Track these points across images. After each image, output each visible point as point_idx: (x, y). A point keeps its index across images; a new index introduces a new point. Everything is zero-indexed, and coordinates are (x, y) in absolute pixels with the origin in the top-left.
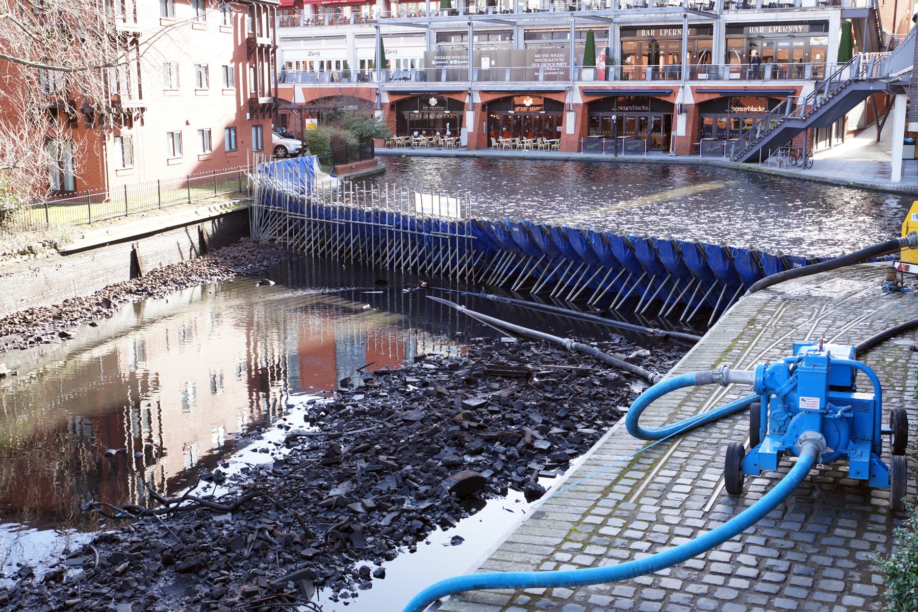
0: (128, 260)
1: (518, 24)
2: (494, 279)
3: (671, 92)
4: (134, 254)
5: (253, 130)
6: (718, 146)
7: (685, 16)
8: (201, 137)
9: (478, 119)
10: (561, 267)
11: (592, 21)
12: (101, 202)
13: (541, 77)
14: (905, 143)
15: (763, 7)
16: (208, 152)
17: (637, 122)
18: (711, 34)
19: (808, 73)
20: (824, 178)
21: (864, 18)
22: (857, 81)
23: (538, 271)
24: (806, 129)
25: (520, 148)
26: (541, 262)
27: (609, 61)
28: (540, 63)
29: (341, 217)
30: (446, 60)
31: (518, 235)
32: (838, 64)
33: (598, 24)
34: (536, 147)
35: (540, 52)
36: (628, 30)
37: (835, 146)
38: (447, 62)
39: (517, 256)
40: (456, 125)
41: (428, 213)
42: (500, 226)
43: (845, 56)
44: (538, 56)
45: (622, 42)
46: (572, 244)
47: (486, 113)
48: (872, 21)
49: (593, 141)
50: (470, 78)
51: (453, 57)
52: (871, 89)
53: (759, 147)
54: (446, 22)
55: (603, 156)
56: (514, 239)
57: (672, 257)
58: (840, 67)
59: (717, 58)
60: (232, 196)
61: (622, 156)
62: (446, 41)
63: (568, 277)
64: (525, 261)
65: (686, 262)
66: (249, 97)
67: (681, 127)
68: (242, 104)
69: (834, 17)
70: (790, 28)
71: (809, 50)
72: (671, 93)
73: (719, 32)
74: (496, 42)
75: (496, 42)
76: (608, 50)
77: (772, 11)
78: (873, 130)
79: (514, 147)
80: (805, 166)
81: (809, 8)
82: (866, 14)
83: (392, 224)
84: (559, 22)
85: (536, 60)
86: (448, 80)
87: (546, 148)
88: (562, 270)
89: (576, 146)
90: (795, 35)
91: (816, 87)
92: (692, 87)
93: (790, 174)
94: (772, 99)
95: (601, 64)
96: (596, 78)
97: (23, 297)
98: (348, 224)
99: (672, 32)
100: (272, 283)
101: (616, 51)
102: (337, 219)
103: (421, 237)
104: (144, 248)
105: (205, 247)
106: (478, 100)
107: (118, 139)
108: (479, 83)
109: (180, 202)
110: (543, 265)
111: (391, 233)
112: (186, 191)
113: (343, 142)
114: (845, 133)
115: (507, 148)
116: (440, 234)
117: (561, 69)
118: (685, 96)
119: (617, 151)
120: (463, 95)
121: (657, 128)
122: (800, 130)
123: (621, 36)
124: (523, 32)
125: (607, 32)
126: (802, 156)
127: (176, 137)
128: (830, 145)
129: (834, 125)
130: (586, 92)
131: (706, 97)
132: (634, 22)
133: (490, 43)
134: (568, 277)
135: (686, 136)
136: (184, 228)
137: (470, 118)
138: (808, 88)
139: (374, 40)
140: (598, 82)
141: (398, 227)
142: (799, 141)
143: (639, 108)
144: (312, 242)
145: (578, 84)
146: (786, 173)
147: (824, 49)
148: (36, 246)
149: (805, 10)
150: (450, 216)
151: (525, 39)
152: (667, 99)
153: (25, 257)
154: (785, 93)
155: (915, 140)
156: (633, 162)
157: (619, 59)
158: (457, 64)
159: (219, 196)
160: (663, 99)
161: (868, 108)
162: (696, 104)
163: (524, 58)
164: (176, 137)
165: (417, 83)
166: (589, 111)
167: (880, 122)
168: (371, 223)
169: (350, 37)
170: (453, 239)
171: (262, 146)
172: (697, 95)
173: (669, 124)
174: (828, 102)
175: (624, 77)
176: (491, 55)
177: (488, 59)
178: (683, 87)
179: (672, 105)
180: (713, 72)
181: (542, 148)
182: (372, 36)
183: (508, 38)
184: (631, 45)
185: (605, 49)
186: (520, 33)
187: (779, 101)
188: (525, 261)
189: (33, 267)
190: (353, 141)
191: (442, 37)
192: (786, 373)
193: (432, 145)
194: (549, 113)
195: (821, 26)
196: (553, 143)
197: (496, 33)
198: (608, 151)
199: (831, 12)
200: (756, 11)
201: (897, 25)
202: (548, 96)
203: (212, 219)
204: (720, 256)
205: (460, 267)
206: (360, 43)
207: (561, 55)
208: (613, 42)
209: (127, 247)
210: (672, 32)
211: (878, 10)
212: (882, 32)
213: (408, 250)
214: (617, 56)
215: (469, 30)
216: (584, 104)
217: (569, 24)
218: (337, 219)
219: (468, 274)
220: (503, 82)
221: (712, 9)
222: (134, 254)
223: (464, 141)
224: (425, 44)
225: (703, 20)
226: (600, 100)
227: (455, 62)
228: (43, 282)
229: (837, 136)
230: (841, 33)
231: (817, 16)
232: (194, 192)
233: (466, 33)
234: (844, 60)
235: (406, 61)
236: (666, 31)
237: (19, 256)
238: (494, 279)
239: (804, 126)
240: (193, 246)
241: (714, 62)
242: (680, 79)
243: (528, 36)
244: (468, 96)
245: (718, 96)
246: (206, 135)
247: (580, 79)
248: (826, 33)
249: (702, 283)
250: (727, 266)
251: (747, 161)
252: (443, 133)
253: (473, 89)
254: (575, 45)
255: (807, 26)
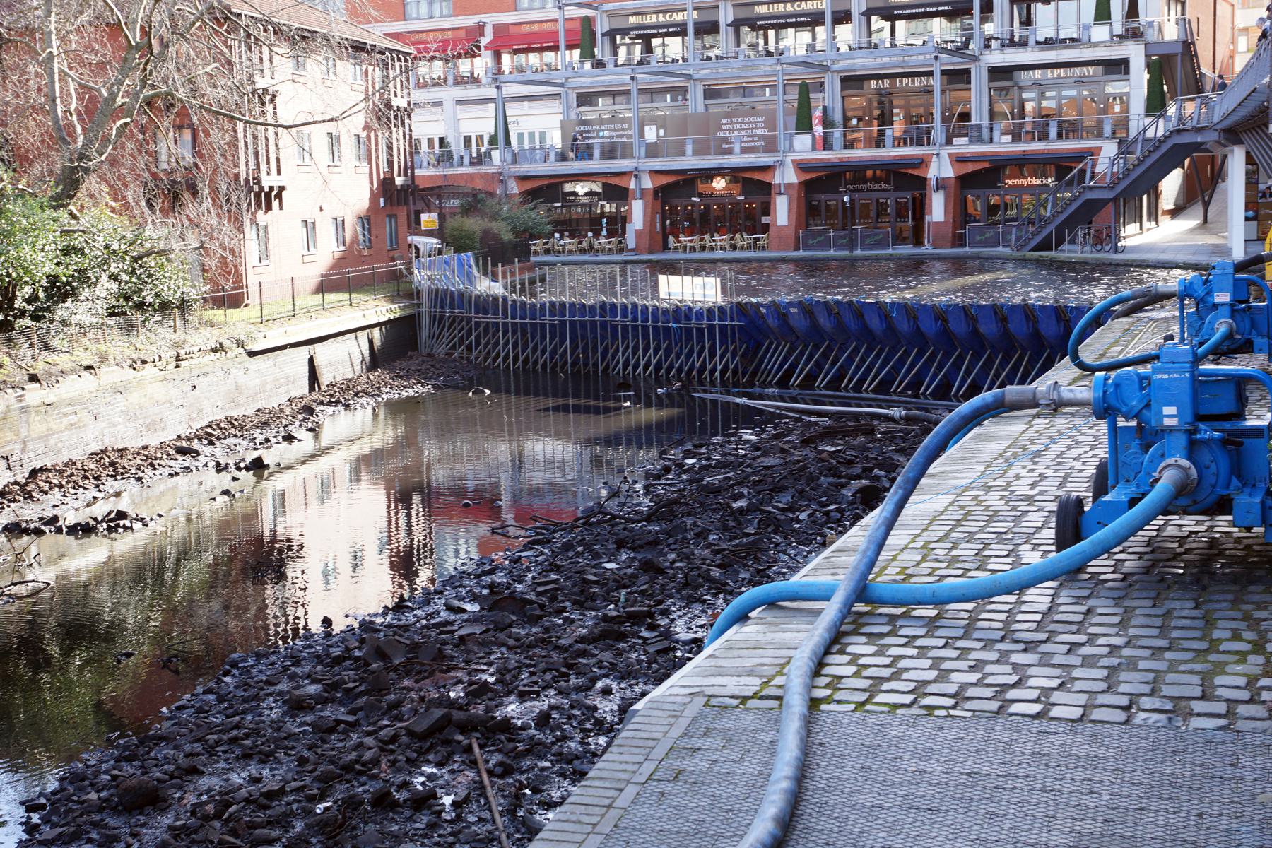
0: (306, 369)
1: (696, 77)
2: (764, 376)
3: (922, 163)
4: (311, 361)
5: (387, 220)
6: (990, 234)
7: (936, 58)
8: (334, 228)
9: (649, 210)
10: (849, 356)
11: (801, 69)
12: (239, 307)
13: (737, 148)
14: (1247, 219)
15: (1038, 43)
16: (342, 248)
17: (873, 208)
18: (969, 82)
19: (1107, 130)
20: (1144, 261)
21: (1177, 54)
22: (1178, 132)
23: (819, 366)
24: (1115, 199)
25: (712, 249)
26: (823, 353)
27: (827, 123)
28: (729, 130)
29: (552, 314)
30: (594, 131)
31: (796, 317)
32: (1147, 116)
33: (810, 73)
34: (734, 247)
35: (728, 115)
36: (852, 82)
37: (1148, 230)
38: (594, 135)
39: (792, 343)
40: (618, 224)
41: (676, 297)
42: (772, 308)
43: (1156, 105)
44: (725, 121)
45: (843, 98)
46: (868, 322)
47: (659, 203)
48: (1187, 58)
49: (814, 235)
50: (636, 154)
51: (603, 127)
52: (1199, 140)
53: (1051, 228)
54: (589, 78)
55: (832, 252)
56: (791, 322)
57: (994, 325)
58: (1148, 120)
59: (979, 117)
60: (392, 299)
61: (858, 252)
62: (591, 105)
63: (858, 368)
64: (802, 354)
65: (1011, 330)
66: (382, 177)
67: (937, 209)
68: (375, 185)
69: (1135, 54)
70: (1077, 71)
71: (1107, 101)
72: (921, 163)
73: (979, 80)
74: (663, 104)
75: (663, 104)
76: (825, 108)
77: (1051, 49)
78: (1198, 209)
79: (703, 248)
80: (1116, 251)
81: (1102, 42)
82: (1179, 49)
83: (627, 317)
84: (749, 73)
85: (724, 127)
86: (603, 157)
87: (749, 248)
88: (850, 360)
89: (792, 242)
90: (1084, 80)
91: (1119, 148)
92: (950, 155)
93: (1097, 259)
94: (1062, 166)
95: (818, 130)
96: (814, 148)
97: (218, 404)
98: (563, 323)
99: (913, 81)
100: (488, 392)
101: (836, 110)
102: (547, 317)
103: (667, 329)
104: (323, 353)
105: (376, 360)
106: (648, 184)
107: (254, 228)
108: (648, 160)
109: (335, 305)
110: (825, 356)
111: (625, 328)
112: (321, 295)
113: (496, 237)
114: (1160, 213)
115: (693, 249)
116: (693, 323)
117: (762, 137)
118: (941, 168)
119: (852, 245)
120: (625, 178)
121: (900, 214)
122: (1105, 202)
123: (842, 90)
124: (702, 88)
125: (822, 84)
126: (1110, 237)
127: (310, 227)
128: (1141, 229)
129: (1145, 197)
130: (802, 167)
131: (971, 168)
132: (860, 70)
133: (655, 105)
134: (858, 368)
135: (946, 222)
136: (353, 335)
137: (638, 211)
138: (1109, 149)
139: (492, 106)
140: (817, 152)
141: (635, 319)
142: (1102, 219)
143: (877, 187)
144: (510, 346)
145: (790, 157)
146: (1092, 259)
147: (1125, 100)
148: (227, 344)
149: (1096, 45)
150: (707, 300)
151: (705, 99)
152: (916, 172)
153: (218, 354)
154: (1079, 157)
155: (1256, 210)
156: (877, 259)
157: (841, 122)
158: (609, 137)
159: (379, 300)
160: (910, 171)
161: (1188, 180)
162: (957, 178)
163: (707, 123)
164: (310, 227)
165: (559, 164)
166: (806, 194)
167: (1206, 199)
168: (597, 319)
169: (448, 105)
170: (711, 328)
171: (397, 243)
172: (957, 165)
173: (920, 208)
174: (1159, 147)
175: (849, 144)
176: (660, 123)
177: (654, 128)
178: (938, 154)
179: (923, 181)
180: (975, 134)
181: (742, 248)
182: (492, 100)
183: (680, 98)
184: (858, 101)
185: (821, 108)
186: (698, 90)
187: (1071, 169)
188: (802, 354)
189: (225, 368)
190: (508, 236)
191: (585, 99)
192: (1201, 283)
193: (583, 251)
194: (750, 199)
195: (1119, 67)
196: (758, 239)
197: (664, 90)
198: (838, 247)
199: (1131, 47)
200: (1029, 49)
201: (1218, 65)
202: (748, 175)
203: (379, 325)
204: (1054, 317)
205: (722, 357)
206: (463, 111)
207: (759, 119)
208: (830, 98)
209: (304, 352)
210: (913, 81)
211: (1193, 43)
212: (1200, 73)
213: (639, 358)
214: (838, 117)
215: (633, 88)
216: (800, 183)
217: (775, 75)
218: (547, 317)
219: (732, 367)
220: (684, 158)
221: (967, 48)
222: (311, 361)
223: (631, 241)
224: (561, 111)
225: (958, 63)
226: (821, 177)
227: (607, 133)
228: (234, 387)
229: (1149, 220)
230: (1147, 76)
231: (1113, 53)
232: (330, 297)
233: (627, 92)
234: (1155, 110)
235: (532, 135)
236: (905, 80)
237: (212, 354)
238: (764, 376)
239: (1111, 195)
240: (363, 360)
241: (974, 121)
242: (929, 144)
243: (710, 94)
244: (633, 179)
245: (987, 165)
246: (340, 224)
247: (791, 149)
248: (1126, 77)
249: (1030, 355)
250: (1062, 329)
251: (1035, 249)
252: (597, 234)
253: (640, 169)
254: (783, 104)
255: (1100, 68)
